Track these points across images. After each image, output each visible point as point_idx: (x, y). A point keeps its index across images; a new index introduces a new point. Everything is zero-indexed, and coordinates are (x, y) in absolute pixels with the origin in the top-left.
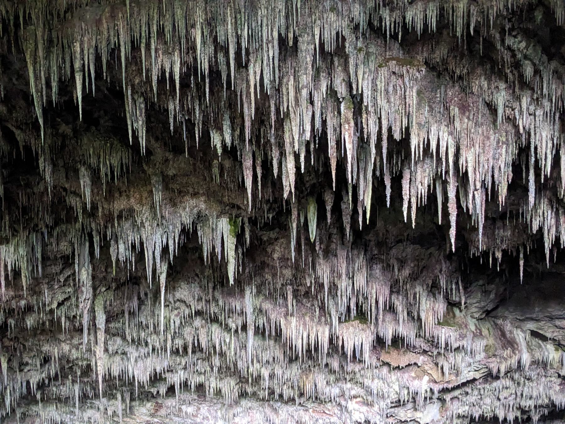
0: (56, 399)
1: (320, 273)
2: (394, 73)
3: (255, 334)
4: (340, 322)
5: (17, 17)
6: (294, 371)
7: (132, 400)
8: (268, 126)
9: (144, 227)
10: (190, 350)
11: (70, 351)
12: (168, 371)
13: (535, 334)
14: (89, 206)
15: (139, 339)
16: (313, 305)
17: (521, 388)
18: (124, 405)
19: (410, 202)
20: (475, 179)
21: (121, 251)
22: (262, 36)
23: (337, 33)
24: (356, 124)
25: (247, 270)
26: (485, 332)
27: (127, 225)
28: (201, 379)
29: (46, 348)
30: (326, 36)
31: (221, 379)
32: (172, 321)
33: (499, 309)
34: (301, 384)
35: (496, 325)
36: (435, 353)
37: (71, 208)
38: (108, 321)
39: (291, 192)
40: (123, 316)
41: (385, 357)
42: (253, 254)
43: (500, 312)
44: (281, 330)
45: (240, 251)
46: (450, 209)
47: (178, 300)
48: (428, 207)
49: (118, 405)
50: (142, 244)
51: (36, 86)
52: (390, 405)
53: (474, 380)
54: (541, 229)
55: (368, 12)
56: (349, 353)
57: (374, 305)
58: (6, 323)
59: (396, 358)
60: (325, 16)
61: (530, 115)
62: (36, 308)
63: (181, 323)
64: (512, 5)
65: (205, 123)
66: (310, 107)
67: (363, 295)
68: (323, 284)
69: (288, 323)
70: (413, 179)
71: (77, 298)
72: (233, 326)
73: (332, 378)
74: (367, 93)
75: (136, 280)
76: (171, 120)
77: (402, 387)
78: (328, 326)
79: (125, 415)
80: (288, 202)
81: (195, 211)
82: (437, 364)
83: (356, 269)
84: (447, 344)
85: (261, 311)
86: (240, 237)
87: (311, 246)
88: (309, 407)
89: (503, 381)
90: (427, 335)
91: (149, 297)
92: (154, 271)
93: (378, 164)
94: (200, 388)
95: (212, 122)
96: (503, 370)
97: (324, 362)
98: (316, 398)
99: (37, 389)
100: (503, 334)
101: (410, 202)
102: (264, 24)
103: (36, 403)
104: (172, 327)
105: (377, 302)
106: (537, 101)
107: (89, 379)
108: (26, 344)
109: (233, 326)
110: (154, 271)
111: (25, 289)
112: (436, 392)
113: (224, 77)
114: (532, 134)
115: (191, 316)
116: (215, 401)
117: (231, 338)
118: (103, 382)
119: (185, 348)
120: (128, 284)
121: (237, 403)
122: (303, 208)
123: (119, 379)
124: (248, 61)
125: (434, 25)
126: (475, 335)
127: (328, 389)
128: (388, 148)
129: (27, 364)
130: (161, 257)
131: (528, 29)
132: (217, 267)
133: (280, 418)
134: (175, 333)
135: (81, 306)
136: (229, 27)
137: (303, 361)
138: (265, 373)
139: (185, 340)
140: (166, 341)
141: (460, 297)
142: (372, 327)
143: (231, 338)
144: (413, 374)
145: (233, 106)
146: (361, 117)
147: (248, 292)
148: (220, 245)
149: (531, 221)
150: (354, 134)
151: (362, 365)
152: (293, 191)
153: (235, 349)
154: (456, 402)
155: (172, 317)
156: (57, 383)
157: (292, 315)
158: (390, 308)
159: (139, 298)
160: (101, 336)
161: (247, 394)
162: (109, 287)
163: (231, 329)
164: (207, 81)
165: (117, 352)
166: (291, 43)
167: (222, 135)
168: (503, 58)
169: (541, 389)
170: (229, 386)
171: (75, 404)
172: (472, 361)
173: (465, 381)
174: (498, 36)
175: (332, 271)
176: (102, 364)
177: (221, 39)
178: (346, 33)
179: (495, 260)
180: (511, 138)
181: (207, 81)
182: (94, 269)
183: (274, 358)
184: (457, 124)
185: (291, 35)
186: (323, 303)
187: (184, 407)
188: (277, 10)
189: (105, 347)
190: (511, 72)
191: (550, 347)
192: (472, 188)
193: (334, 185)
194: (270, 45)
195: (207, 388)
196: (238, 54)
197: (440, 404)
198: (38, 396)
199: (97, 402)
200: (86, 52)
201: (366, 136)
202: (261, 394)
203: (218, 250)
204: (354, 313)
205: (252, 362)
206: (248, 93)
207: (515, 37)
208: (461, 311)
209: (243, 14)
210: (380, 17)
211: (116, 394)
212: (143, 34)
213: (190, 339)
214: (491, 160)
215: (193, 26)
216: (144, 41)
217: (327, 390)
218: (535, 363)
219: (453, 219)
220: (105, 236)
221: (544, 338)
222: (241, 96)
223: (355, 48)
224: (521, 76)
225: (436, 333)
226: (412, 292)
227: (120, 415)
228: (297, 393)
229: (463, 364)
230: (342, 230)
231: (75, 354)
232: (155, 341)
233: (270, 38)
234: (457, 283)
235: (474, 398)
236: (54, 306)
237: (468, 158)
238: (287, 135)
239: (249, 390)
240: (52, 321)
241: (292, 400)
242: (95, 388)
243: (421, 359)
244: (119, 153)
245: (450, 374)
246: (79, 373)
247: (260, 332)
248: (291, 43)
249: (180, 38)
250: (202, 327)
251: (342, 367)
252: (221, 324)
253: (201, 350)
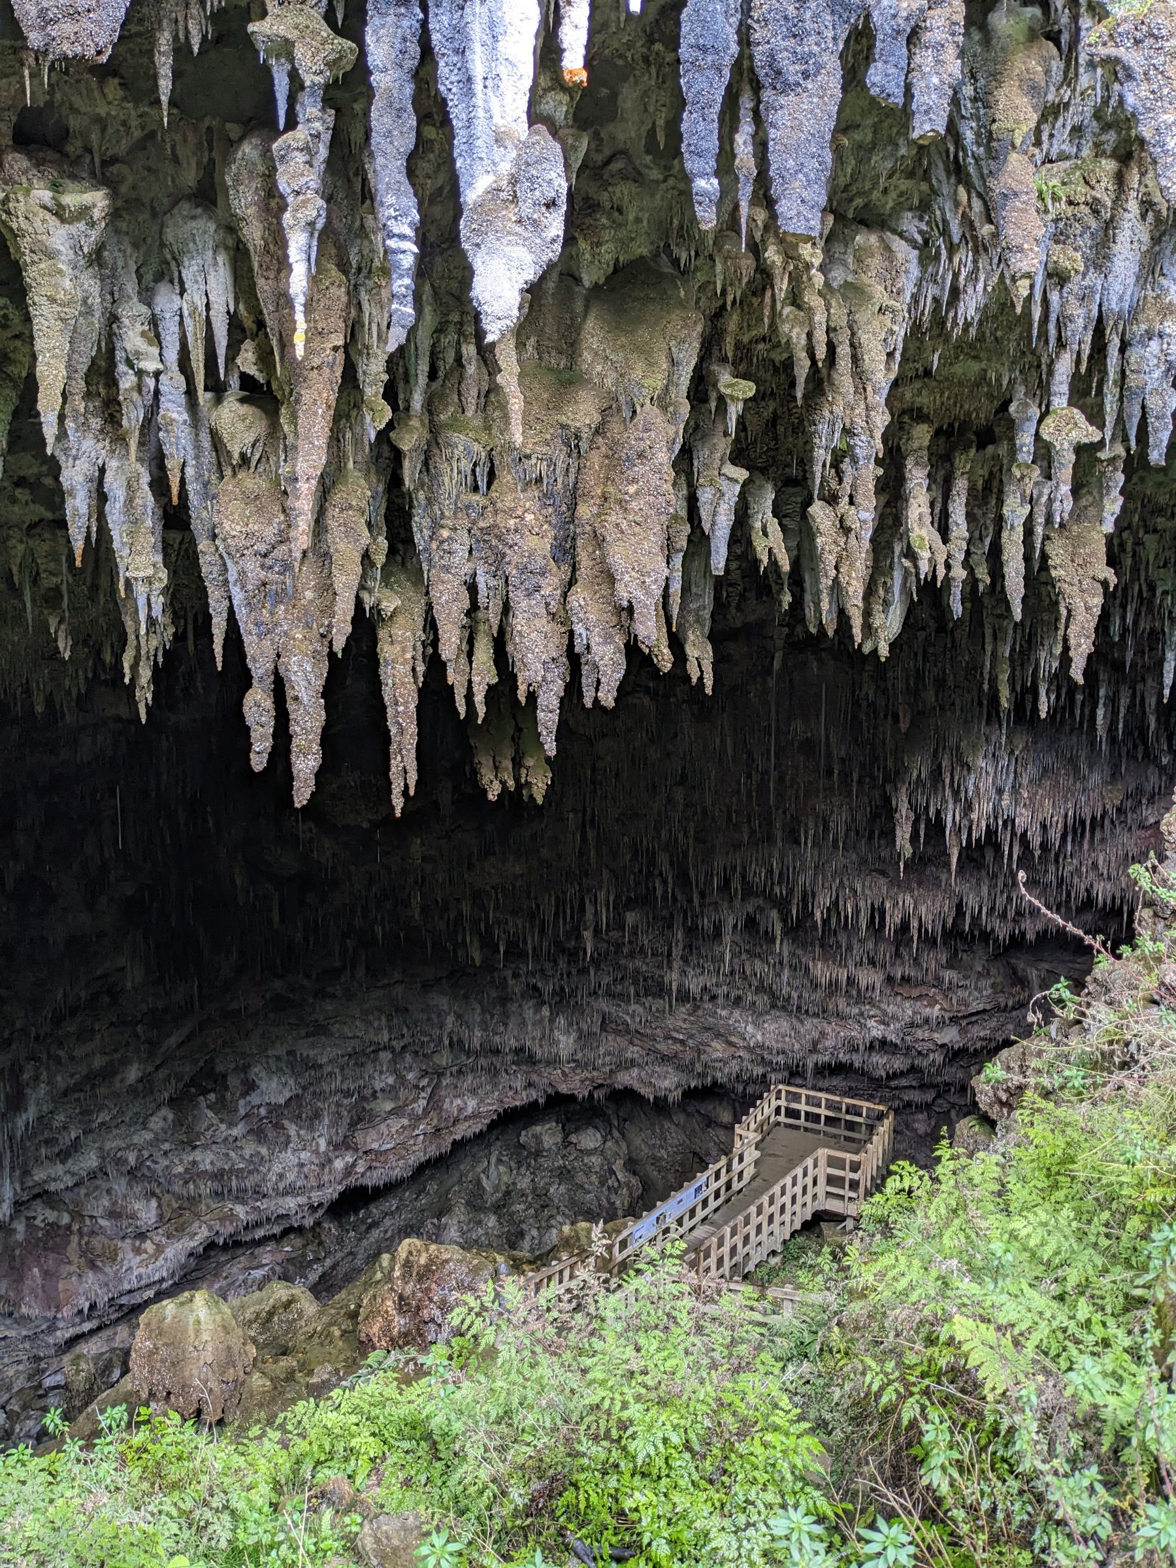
26: (993, 971)
59: (904, 991)
69: (815, 966)
77: (914, 1013)
100: (1015, 972)
111: (164, 99)
121: (767, 1013)
170: (762, 1000)
241: (816, 1015)
247: (793, 968)
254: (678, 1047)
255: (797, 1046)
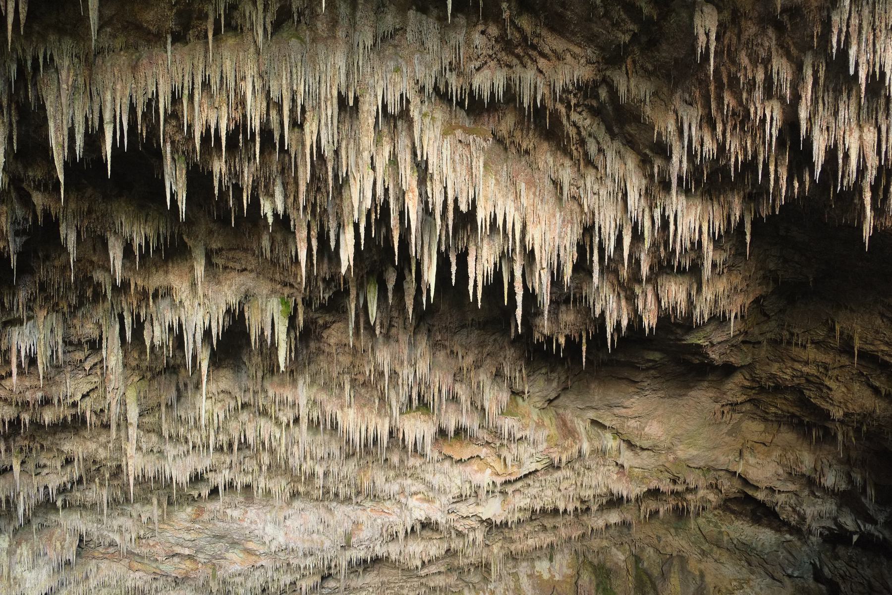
0: (80, 506)
1: (380, 360)
2: (460, 141)
3: (308, 428)
4: (401, 413)
5: (35, 60)
6: (350, 468)
7: (170, 503)
8: (325, 194)
9: (184, 307)
10: (235, 447)
11: (96, 450)
12: (211, 471)
13: (594, 422)
14: (118, 282)
15: (178, 435)
16: (373, 396)
17: (580, 478)
18: (160, 510)
19: (475, 281)
20: (542, 259)
21: (155, 334)
22: (319, 93)
23: (402, 95)
24: (420, 195)
25: (300, 358)
26: (547, 422)
27: (164, 304)
28: (248, 479)
29: (67, 447)
30: (389, 97)
31: (270, 478)
32: (215, 415)
33: (561, 398)
34: (359, 482)
35: (558, 414)
36: (498, 445)
37: (99, 284)
38: (141, 415)
39: (349, 265)
40: (159, 410)
41: (447, 451)
42: (306, 337)
43: (563, 400)
44: (337, 423)
45: (292, 335)
46: (516, 289)
47: (222, 391)
48: (494, 286)
49: (153, 511)
50: (180, 326)
51: (57, 138)
52: (452, 500)
53: (536, 471)
54: (603, 313)
55: (433, 76)
56: (410, 447)
57: (436, 394)
58: (18, 418)
60: (388, 77)
61: (595, 194)
62: (56, 401)
63: (226, 417)
64: (578, 80)
65: (255, 188)
66: (371, 172)
67: (426, 383)
68: (383, 372)
70: (479, 257)
71: (105, 388)
72: (284, 420)
73: (392, 474)
74: (433, 161)
75: (173, 369)
76: (216, 184)
78: (388, 418)
79: (162, 521)
80: (346, 282)
81: (243, 289)
82: (499, 456)
83: (418, 355)
84: (510, 434)
85: (315, 402)
86: (292, 319)
87: (370, 329)
88: (367, 505)
89: (564, 472)
90: (491, 425)
91: (189, 387)
92: (194, 357)
93: (443, 238)
94: (248, 487)
95: (262, 186)
96: (564, 460)
97: (384, 457)
98: (375, 496)
99: (57, 495)
101: (475, 281)
102: (323, 81)
103: (57, 510)
104: (216, 421)
105: (440, 391)
106: (600, 180)
107: (120, 482)
108: (44, 443)
109: (284, 420)
110: (194, 357)
111: (41, 377)
112: (498, 485)
113: (277, 136)
114: (597, 214)
115: (236, 409)
116: (265, 503)
117: (281, 433)
118: (135, 485)
119: (230, 445)
120: (165, 370)
121: (289, 504)
122: (361, 287)
123: (155, 482)
124: (304, 119)
125: (501, 93)
126: (538, 425)
127: (387, 485)
128: (454, 220)
129: (45, 466)
130: (203, 341)
131: (592, 106)
132: (266, 354)
133: (336, 519)
134: (219, 428)
135: (108, 397)
136: (284, 82)
137: (361, 456)
138: (320, 470)
139: (229, 435)
140: (208, 437)
141: (523, 386)
142: (435, 418)
143: (281, 433)
144: (475, 467)
145: (287, 172)
146: (426, 187)
147: (301, 382)
148: (270, 327)
149: (594, 305)
150: (419, 205)
151: (423, 460)
152: (352, 264)
153: (287, 445)
154: (517, 496)
155: (216, 410)
156: (81, 487)
157: (350, 406)
158: (453, 398)
159: (178, 390)
160: (133, 432)
161: (298, 493)
162: (143, 377)
163: (281, 423)
164: (258, 139)
165: (152, 451)
166: (351, 104)
167: (274, 202)
168: (568, 134)
169: (600, 478)
170: (279, 485)
171: (103, 511)
172: (534, 451)
173: (527, 472)
174: (563, 110)
175: (393, 358)
176: (135, 463)
177: (274, 95)
178: (411, 95)
179: (558, 345)
180: (577, 218)
181: (258, 139)
182: (125, 356)
183: (329, 454)
184: (524, 200)
185: (351, 95)
186: (383, 393)
187: (229, 511)
188: (337, 67)
189: (137, 445)
190: (577, 149)
191: (609, 435)
192: (538, 266)
193: (396, 259)
194: (329, 103)
195: (255, 488)
196: (292, 111)
197: (502, 498)
198: (59, 503)
199: (129, 508)
200: (118, 101)
201: (430, 207)
202: (315, 494)
203: (268, 332)
204: (415, 403)
205: (305, 458)
206: (304, 155)
207: (580, 113)
208: (524, 400)
209: (299, 69)
210: (446, 82)
211: (151, 498)
212: (186, 85)
213: (236, 435)
214: (557, 239)
215: (244, 78)
216: (186, 92)
217: (387, 487)
218: (595, 452)
219: (519, 298)
220: (138, 316)
221: (604, 427)
222: (295, 158)
223: (420, 113)
224: (586, 154)
225: (499, 423)
226: (476, 381)
227: (156, 521)
228: (353, 491)
229: (526, 455)
230: (403, 309)
231: (102, 454)
232: (195, 437)
233: (329, 96)
234: (520, 371)
235: (536, 490)
236: (78, 398)
237: (535, 235)
238: (346, 203)
239: (302, 489)
240: (74, 415)
241: (348, 499)
242: (126, 493)
243: (484, 452)
244: (156, 222)
245: (512, 466)
246: (107, 476)
247: (314, 426)
248: (351, 104)
249: (228, 92)
250: (250, 421)
251: (402, 461)
252: (271, 417)
253: (248, 447)
254: (188, 565)
255: (327, 544)
